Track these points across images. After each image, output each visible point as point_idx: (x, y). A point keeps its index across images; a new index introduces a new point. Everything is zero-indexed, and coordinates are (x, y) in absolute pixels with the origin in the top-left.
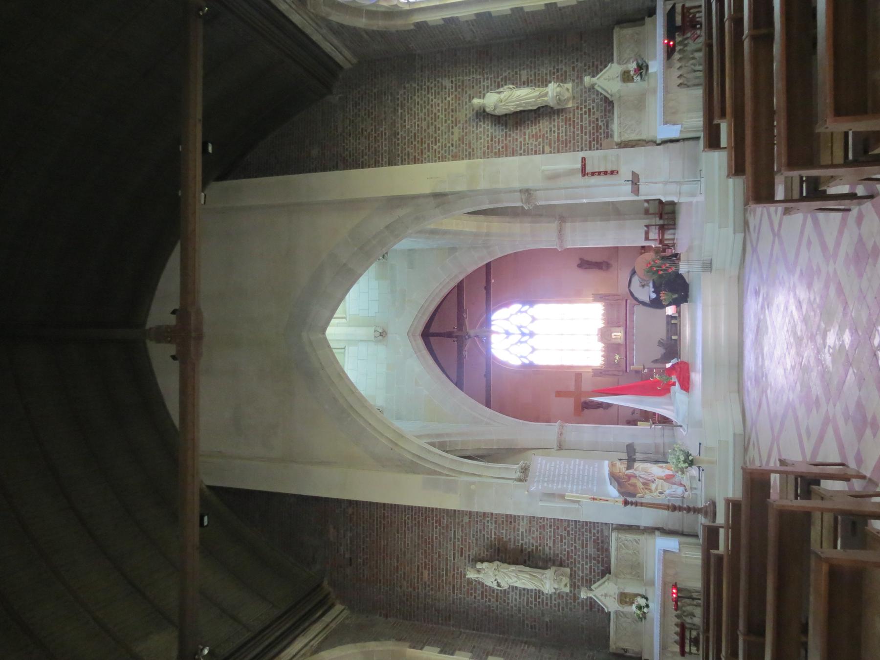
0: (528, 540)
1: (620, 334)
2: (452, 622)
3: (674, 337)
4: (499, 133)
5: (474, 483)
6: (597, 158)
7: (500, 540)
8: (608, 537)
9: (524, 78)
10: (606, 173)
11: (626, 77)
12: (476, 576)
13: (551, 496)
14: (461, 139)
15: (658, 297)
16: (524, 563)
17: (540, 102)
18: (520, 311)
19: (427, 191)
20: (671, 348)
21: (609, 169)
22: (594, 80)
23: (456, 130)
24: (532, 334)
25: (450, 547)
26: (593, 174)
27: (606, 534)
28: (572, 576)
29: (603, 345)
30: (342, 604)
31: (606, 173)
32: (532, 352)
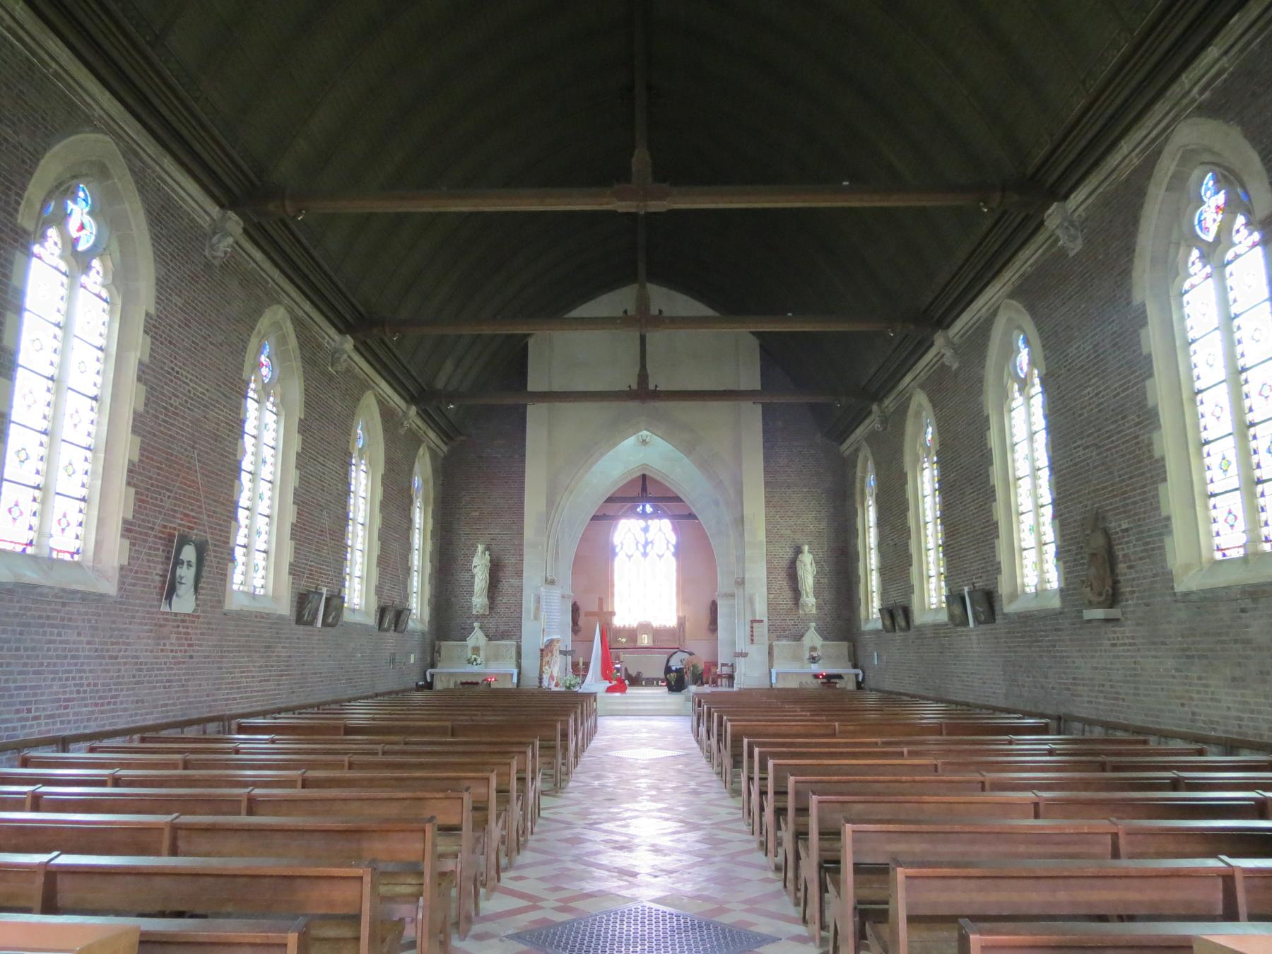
0: (507, 584)
1: (646, 642)
2: (444, 533)
3: (644, 683)
4: (785, 563)
5: (543, 548)
6: (762, 630)
7: (504, 566)
8: (511, 639)
9: (822, 580)
10: (752, 636)
11: (813, 649)
12: (480, 551)
13: (538, 600)
14: (782, 536)
15: (672, 671)
16: (490, 583)
17: (803, 593)
18: (668, 542)
19: (745, 512)
20: (636, 681)
21: (754, 638)
22: (813, 629)
23: (789, 532)
24: (645, 554)
25: (497, 531)
26: (752, 627)
27: (514, 637)
28: (483, 616)
29: (635, 626)
30: (448, 451)
31: (752, 636)
32: (627, 555)
